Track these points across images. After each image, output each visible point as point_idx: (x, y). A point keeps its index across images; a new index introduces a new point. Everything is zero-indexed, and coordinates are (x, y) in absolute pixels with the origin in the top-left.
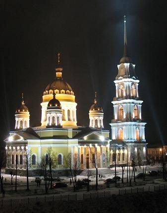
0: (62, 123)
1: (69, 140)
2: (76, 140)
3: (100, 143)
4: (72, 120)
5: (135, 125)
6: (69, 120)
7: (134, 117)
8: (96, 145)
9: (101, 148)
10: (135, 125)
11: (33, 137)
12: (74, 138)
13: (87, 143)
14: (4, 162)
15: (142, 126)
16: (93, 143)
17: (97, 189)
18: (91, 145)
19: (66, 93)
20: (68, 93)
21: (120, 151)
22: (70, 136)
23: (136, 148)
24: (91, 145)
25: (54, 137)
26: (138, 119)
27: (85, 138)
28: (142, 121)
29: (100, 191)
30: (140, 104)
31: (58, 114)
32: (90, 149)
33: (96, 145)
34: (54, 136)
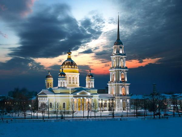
0: (66, 85)
1: (69, 95)
2: (72, 95)
3: (87, 97)
4: (75, 83)
5: (121, 85)
6: (73, 83)
7: (120, 80)
8: (85, 98)
9: (89, 100)
10: (121, 85)
11: (52, 93)
12: (72, 94)
13: (79, 96)
14: (18, 49)
15: (127, 85)
16: (83, 97)
17: (73, 118)
18: (81, 98)
19: (15, 122)
20: (73, 68)
21: (102, 102)
22: (70, 93)
23: (128, 100)
24: (81, 98)
25: (61, 93)
26: (125, 81)
27: (78, 94)
28: (127, 82)
29: (74, 118)
30: (126, 71)
31: (64, 81)
32: (81, 100)
33: (85, 98)
34: (61, 93)
